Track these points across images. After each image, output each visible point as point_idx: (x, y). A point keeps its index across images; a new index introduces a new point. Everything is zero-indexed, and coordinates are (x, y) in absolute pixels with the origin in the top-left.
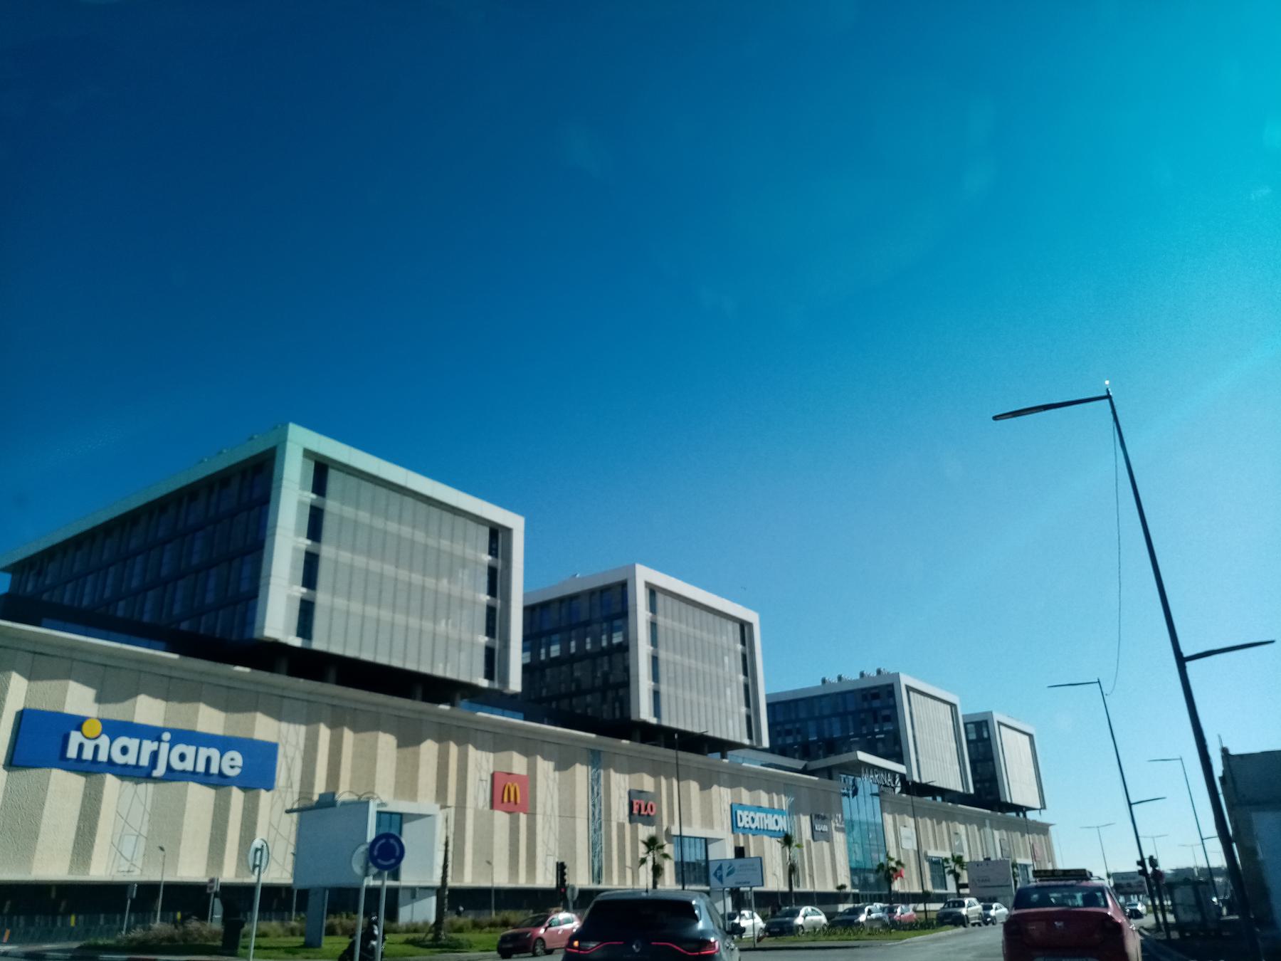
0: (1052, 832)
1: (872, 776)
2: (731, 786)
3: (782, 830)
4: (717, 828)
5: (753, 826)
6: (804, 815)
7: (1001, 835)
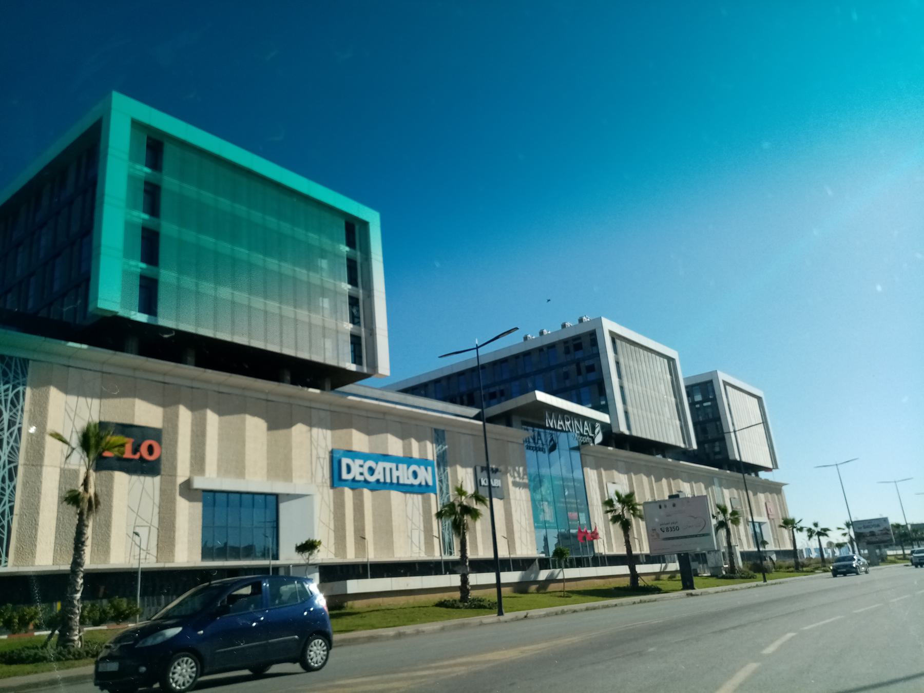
1: (562, 423)
2: (332, 427)
3: (423, 483)
4: (296, 480)
5: (372, 479)
6: (464, 465)
7: (766, 498)
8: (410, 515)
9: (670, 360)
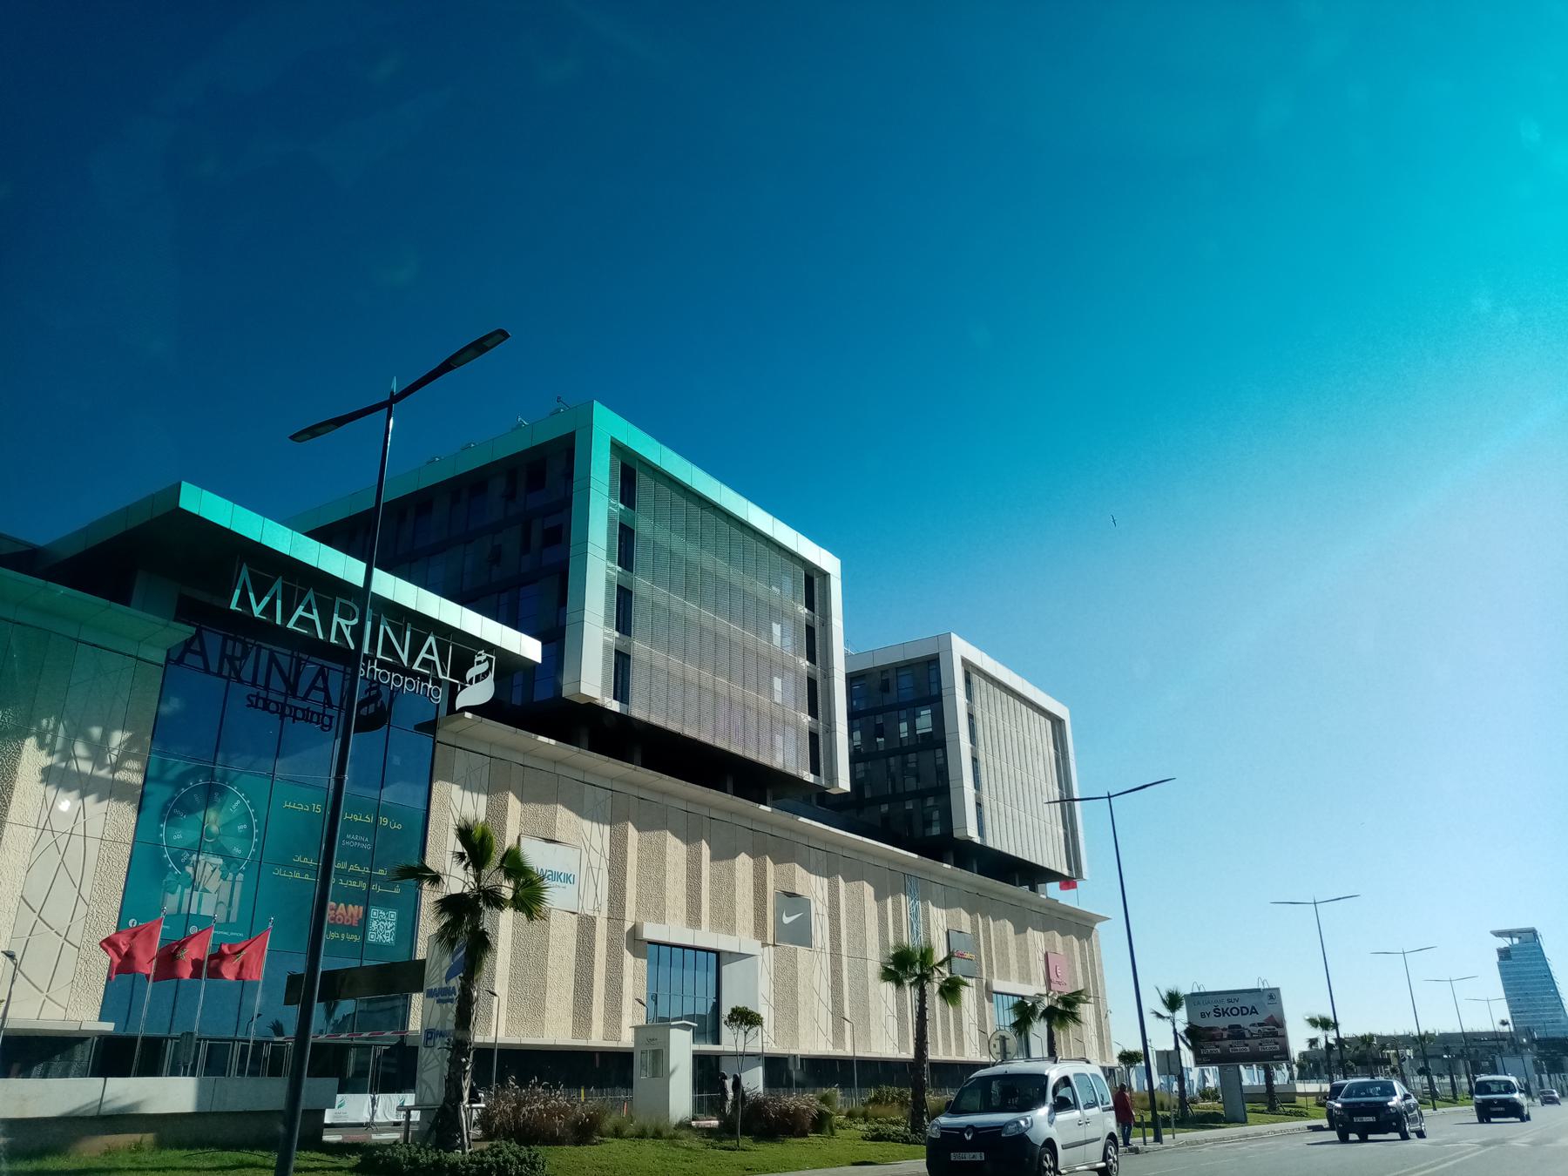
0: (1101, 935)
7: (1050, 943)
8: (816, 986)
9: (1057, 723)
